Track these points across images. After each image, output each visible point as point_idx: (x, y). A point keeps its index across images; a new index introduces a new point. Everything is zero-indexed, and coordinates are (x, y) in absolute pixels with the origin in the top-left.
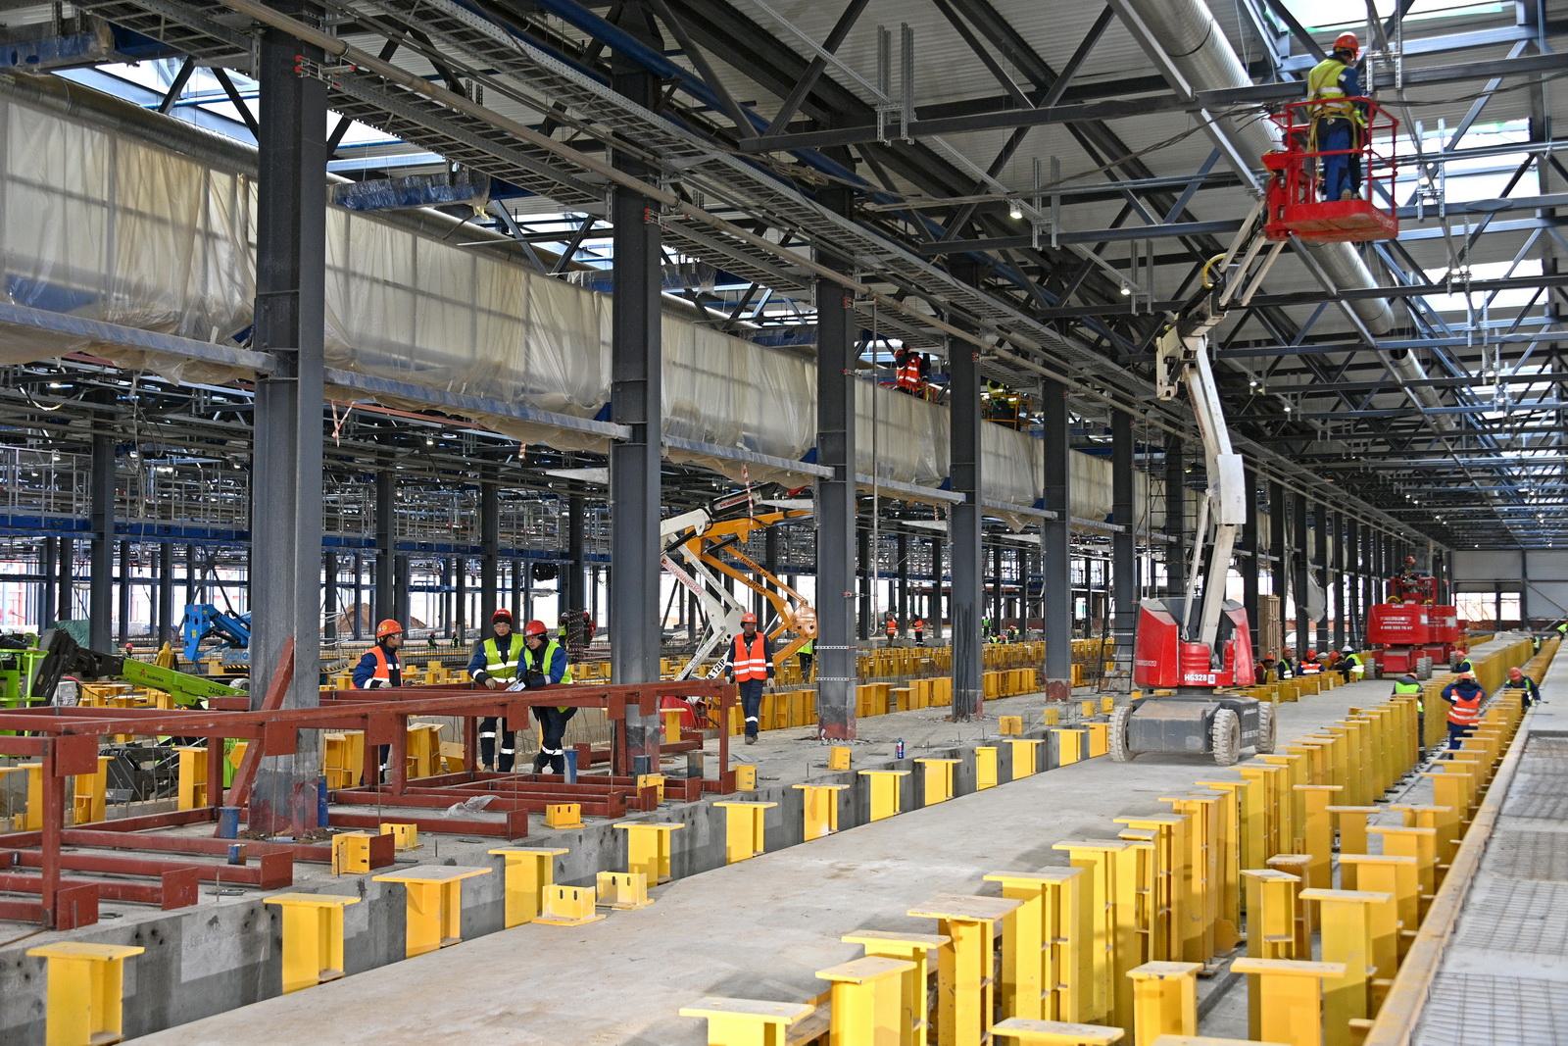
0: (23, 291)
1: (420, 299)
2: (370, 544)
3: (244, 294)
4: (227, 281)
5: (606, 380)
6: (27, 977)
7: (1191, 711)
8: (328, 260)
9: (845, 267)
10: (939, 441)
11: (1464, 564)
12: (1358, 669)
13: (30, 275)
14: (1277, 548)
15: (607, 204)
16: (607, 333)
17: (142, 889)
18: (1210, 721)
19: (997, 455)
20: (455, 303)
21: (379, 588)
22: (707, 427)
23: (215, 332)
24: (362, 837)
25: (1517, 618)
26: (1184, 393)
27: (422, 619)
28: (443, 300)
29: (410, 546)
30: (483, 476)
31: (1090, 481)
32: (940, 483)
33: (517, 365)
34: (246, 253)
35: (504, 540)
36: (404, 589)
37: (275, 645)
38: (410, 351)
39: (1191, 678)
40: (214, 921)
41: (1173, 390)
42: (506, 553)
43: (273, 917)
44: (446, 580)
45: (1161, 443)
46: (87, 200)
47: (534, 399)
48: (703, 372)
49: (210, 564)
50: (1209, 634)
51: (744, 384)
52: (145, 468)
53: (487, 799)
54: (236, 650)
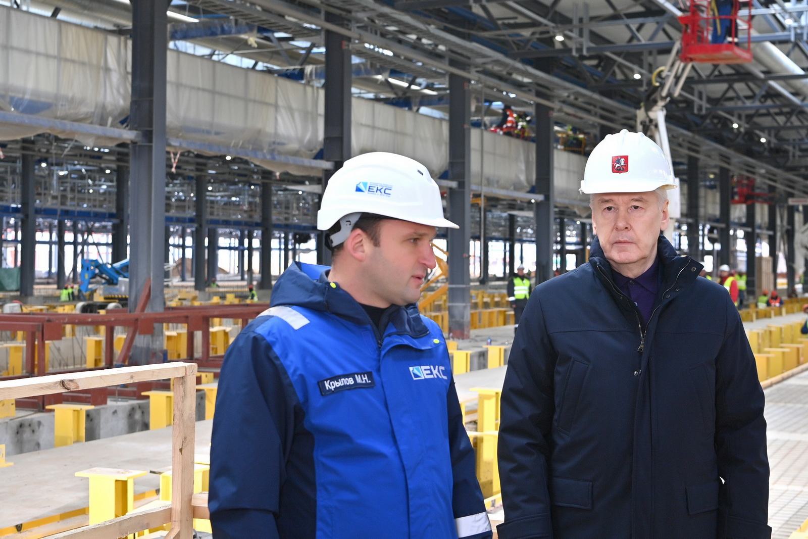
0: (17, 103)
2: (191, 220)
3: (124, 99)
4: (116, 92)
5: (321, 136)
6: (33, 431)
10: (527, 163)
13: (20, 96)
14: (772, 226)
15: (321, 38)
16: (321, 109)
17: (81, 397)
21: (198, 247)
23: (110, 120)
27: (226, 269)
30: (263, 178)
32: (528, 189)
33: (270, 129)
34: (125, 78)
35: (276, 217)
36: (214, 247)
40: (115, 412)
42: (279, 227)
43: (143, 413)
44: (241, 243)
45: (684, 160)
46: (47, 56)
47: (280, 148)
48: (379, 129)
49: (90, 232)
52: (51, 174)
54: (111, 287)
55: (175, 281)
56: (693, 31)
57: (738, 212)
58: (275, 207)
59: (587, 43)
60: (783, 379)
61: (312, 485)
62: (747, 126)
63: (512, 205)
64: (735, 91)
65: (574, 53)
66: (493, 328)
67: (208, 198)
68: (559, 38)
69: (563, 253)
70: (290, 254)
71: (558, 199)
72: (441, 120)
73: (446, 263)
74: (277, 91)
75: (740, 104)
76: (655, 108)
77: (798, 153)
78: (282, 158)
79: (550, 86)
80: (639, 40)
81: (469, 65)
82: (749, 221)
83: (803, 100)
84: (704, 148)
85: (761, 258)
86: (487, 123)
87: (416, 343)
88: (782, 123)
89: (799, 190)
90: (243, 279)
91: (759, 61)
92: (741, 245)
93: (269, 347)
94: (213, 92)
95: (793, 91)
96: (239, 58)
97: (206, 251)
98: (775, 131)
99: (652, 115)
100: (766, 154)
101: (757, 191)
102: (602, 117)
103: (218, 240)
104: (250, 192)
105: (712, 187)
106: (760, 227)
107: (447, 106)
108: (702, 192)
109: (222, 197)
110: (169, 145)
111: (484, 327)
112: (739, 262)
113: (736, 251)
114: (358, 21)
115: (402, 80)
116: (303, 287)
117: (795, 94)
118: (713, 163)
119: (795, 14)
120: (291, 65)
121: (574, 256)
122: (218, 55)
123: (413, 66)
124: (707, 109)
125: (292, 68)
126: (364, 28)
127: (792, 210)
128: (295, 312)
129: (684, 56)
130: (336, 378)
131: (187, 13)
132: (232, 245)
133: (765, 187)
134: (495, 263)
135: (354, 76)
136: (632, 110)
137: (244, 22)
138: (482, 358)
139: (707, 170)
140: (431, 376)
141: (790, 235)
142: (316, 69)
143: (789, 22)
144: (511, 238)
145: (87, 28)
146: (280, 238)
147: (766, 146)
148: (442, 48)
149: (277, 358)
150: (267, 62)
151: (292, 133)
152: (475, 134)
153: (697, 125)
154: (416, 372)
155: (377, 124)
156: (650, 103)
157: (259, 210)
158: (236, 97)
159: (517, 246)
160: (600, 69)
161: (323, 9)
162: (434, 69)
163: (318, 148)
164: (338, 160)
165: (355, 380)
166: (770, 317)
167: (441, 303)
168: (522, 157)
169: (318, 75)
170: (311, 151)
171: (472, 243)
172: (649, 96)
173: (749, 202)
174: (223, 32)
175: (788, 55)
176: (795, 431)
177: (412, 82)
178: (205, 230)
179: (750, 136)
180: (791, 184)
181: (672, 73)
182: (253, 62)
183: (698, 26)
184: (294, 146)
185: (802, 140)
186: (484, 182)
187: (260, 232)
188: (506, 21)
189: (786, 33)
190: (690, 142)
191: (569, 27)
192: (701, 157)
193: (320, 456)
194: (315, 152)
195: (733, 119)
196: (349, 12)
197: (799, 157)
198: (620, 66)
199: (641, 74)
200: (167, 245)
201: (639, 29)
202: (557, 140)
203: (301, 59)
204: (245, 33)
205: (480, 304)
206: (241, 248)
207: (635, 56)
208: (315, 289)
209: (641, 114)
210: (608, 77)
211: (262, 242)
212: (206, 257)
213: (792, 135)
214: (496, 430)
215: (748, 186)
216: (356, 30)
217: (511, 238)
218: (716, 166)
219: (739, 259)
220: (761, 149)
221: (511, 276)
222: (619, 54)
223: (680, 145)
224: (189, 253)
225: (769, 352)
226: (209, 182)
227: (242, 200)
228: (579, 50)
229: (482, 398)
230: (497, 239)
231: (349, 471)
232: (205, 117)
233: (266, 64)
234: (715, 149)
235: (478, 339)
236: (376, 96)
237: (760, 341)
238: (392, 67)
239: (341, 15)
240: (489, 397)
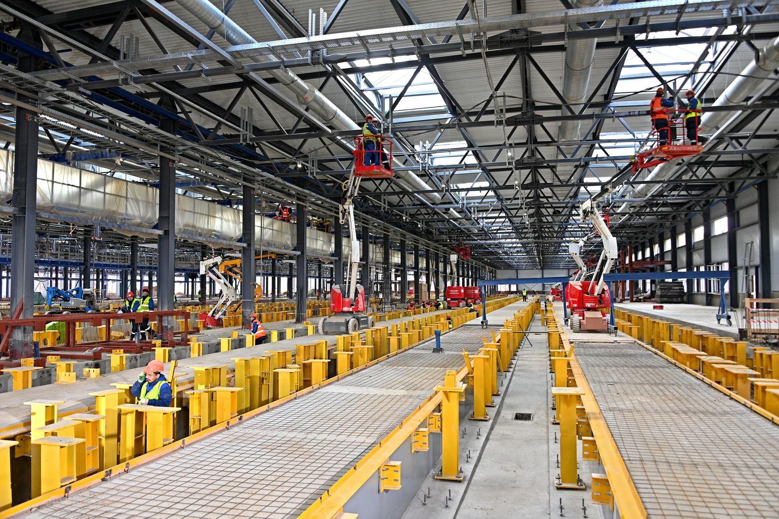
4: (332, 248)
7: (341, 319)
9: (251, 181)
10: (292, 235)
11: (501, 274)
12: (442, 306)
18: (348, 322)
25: (515, 290)
33: (122, 210)
37: (19, 300)
39: (345, 309)
50: (352, 296)
71: (309, 254)
82: (416, 266)
99: (346, 207)
102: (363, 223)
108: (407, 255)
145: (137, 183)
174: (102, 156)
192: (419, 245)
198: (371, 201)
201: (380, 185)
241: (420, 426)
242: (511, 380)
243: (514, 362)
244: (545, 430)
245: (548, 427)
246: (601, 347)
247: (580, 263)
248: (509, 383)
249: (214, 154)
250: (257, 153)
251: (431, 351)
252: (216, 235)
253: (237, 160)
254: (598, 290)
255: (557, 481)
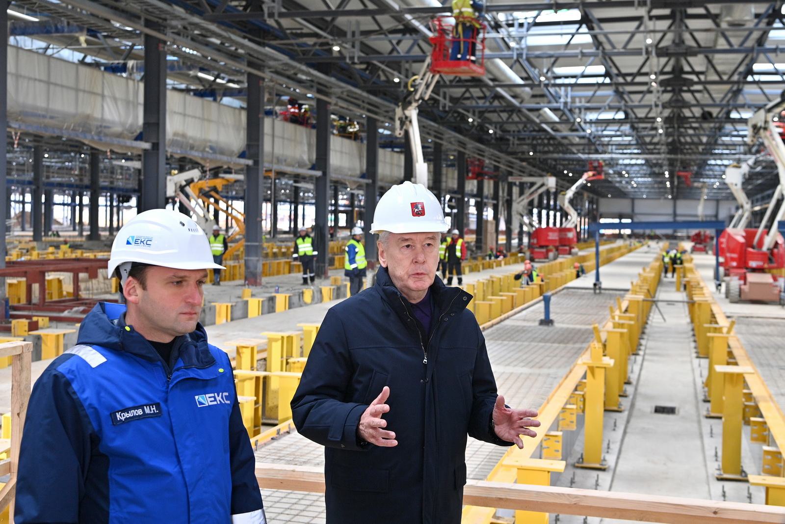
1: (52, 87)
5: (141, 121)
8: (9, 70)
9: (259, 67)
10: (309, 145)
14: (496, 196)
16: (141, 99)
19: (342, 152)
20: (68, 88)
22: (191, 141)
24: (25, 322)
26: (407, 133)
28: (62, 86)
29: (52, 185)
31: (392, 164)
32: (310, 166)
33: (97, 115)
35: (103, 182)
36: (50, 203)
38: (47, 110)
41: (402, 132)
44: (73, 200)
47: (107, 131)
48: (189, 116)
51: (209, 121)
53: (81, 308)
55: (17, 232)
56: (440, 50)
57: (471, 186)
58: (102, 172)
59: (357, 53)
60: (502, 321)
61: (106, 498)
62: (479, 120)
63: (297, 178)
64: (470, 93)
65: (348, 61)
66: (280, 276)
67: (44, 163)
68: (336, 48)
69: (336, 213)
70: (115, 210)
71: (333, 175)
72: (242, 108)
73: (243, 224)
74: (103, 83)
75: (474, 103)
76: (410, 108)
77: (516, 142)
78: (108, 139)
79: (328, 85)
80: (398, 52)
81: (264, 66)
82: (479, 194)
83: (521, 102)
84: (446, 136)
85: (487, 221)
86: (278, 112)
87: (203, 374)
88: (505, 119)
89: (517, 169)
90: (74, 230)
91: (488, 71)
92: (473, 210)
93: (68, 383)
94: (48, 83)
95: (512, 94)
96: (71, 52)
97: (43, 207)
98: (500, 125)
99: (407, 113)
100: (493, 141)
101: (486, 169)
102: (369, 111)
103: (53, 197)
104: (81, 160)
105: (452, 165)
106: (487, 198)
107: (245, 97)
108: (444, 170)
109: (56, 162)
110: (10, 127)
111: (273, 275)
112: (470, 222)
113: (469, 213)
114: (172, 27)
115: (209, 74)
116: (102, 329)
117: (514, 97)
118: (453, 147)
119: (517, 39)
120: (115, 59)
121: (345, 215)
122: (53, 48)
123: (217, 66)
124: (449, 107)
125: (116, 62)
126: (178, 34)
127: (511, 185)
128: (94, 351)
129: (432, 69)
130: (127, 410)
131: (25, 11)
132: (66, 202)
133: (492, 166)
134: (282, 219)
135: (168, 71)
136: (393, 106)
137: (75, 24)
138: (271, 302)
139: (449, 153)
140: (215, 403)
141: (509, 204)
142: (137, 64)
143: (513, 44)
144: (295, 200)
146: (106, 196)
147: (493, 136)
148: (241, 51)
149: (74, 393)
150: (95, 56)
151: (116, 118)
152: (267, 122)
153: (441, 118)
154: (201, 400)
155: (187, 112)
156: (406, 104)
157: (88, 174)
158: (68, 88)
159: (300, 207)
160: (367, 72)
161: (143, 16)
162: (234, 68)
163: (138, 131)
164: (155, 141)
165: (143, 410)
166: (493, 268)
167: (239, 253)
168: (305, 141)
169: (139, 69)
170: (133, 133)
171: (264, 205)
172: (405, 98)
173: (480, 179)
174: (57, 31)
175: (511, 67)
176: (508, 365)
177: (217, 77)
178: (42, 189)
179: (482, 129)
180: (510, 165)
181: (423, 82)
182: (82, 55)
183: (444, 46)
184: (118, 129)
185: (519, 131)
186: (275, 160)
187: (89, 193)
188: (294, 31)
189: (510, 53)
190: (436, 131)
191: (344, 39)
192: (267, 75)
193: (114, 475)
194: (135, 134)
195: (470, 115)
196: (165, 20)
197: (517, 144)
198: (383, 71)
199: (399, 78)
200: (9, 201)
202: (333, 127)
203: (125, 54)
204: (77, 32)
205: (270, 255)
206: (73, 204)
207: (396, 64)
208: (112, 332)
209: (399, 112)
210: (374, 79)
211: (91, 200)
212: (43, 211)
213: (512, 128)
214: (276, 392)
215: (478, 165)
216: (171, 35)
217: (295, 200)
218: (455, 150)
219: (471, 219)
220: (489, 138)
221: (295, 232)
222: (382, 63)
223: (429, 134)
224: (28, 208)
225: (491, 300)
226: (46, 150)
227: (76, 164)
228: (352, 58)
229: (271, 340)
230: (285, 201)
231: (140, 488)
232: (41, 103)
233: (94, 58)
234: (455, 137)
235: (268, 285)
236: (187, 87)
237: (485, 288)
238: (201, 65)
239: (157, 22)
240: (276, 340)
241: (566, 404)
242: (642, 365)
243: (643, 342)
244: (695, 425)
245: (699, 422)
246: (769, 325)
247: (741, 197)
248: (641, 370)
249: (224, 34)
250: (268, 25)
251: (537, 324)
252: (211, 148)
253: (245, 37)
254: (768, 242)
255: (718, 472)
